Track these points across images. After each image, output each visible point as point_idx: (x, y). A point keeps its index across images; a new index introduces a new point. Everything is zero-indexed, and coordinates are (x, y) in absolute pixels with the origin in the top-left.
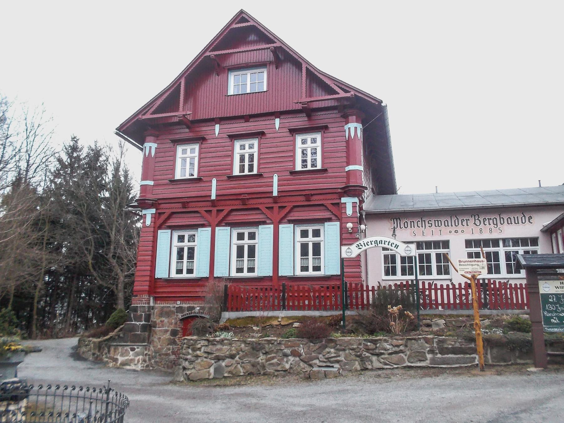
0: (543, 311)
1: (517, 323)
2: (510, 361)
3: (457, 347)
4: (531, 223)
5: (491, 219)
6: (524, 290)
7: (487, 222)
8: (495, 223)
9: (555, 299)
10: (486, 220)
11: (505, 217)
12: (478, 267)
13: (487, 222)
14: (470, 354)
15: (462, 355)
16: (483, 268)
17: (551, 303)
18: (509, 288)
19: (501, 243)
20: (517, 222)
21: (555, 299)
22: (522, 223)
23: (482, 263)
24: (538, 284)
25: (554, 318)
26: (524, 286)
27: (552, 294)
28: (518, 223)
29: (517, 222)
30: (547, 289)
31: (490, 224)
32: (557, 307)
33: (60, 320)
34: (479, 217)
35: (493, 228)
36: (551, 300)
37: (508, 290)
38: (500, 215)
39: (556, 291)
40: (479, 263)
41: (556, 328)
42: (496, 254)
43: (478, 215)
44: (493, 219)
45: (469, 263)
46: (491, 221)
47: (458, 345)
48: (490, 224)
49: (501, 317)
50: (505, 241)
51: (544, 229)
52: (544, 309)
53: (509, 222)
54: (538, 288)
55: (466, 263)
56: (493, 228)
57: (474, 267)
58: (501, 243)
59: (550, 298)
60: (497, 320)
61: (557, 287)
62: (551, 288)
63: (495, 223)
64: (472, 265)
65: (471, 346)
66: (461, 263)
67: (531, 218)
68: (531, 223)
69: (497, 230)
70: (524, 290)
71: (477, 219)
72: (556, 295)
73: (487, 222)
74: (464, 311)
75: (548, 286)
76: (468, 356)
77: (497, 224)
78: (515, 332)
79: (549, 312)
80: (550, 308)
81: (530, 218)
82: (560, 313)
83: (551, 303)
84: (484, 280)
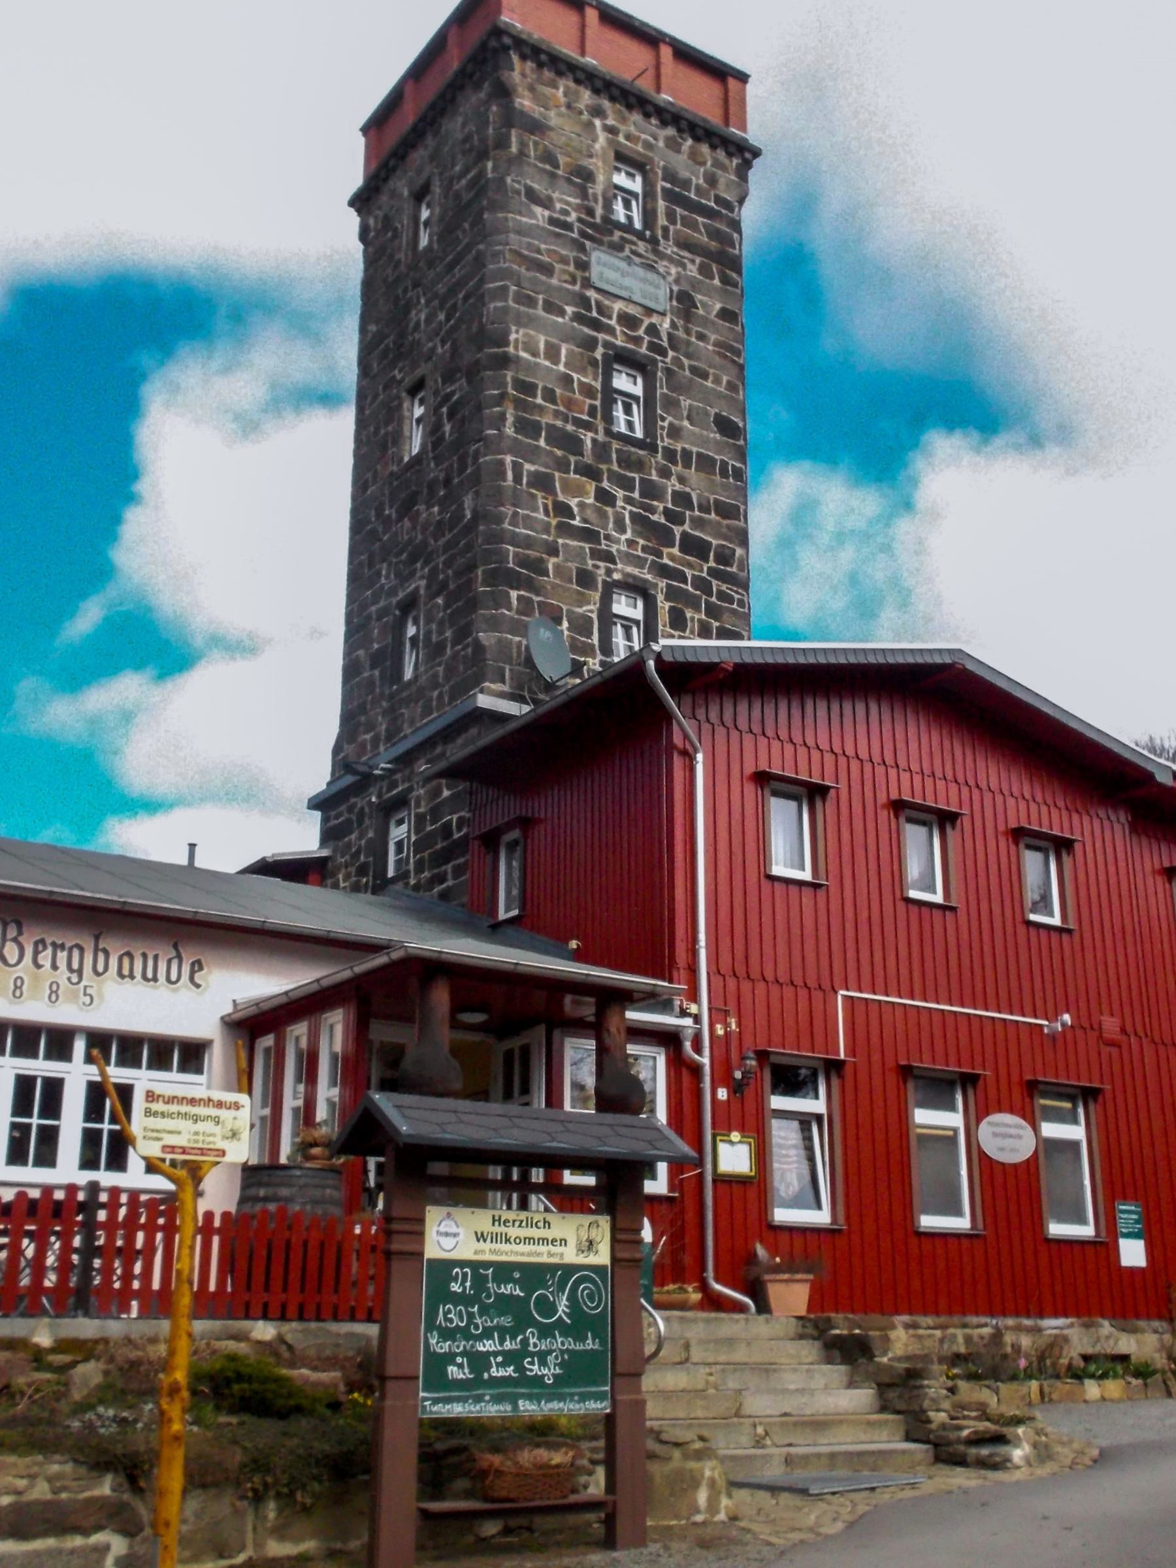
0: (427, 1330)
1: (240, 1377)
2: (242, 1548)
3: (37, 1502)
4: (198, 986)
5: (62, 947)
6: (216, 1240)
7: (45, 958)
8: (75, 966)
9: (468, 1284)
10: (45, 948)
11: (115, 946)
12: (217, 1130)
13: (45, 958)
14: (86, 1532)
15: (51, 1542)
16: (234, 1135)
17: (457, 1299)
18: (143, 1227)
19: (79, 1046)
20: (150, 975)
21: (468, 1284)
22: (168, 980)
23: (232, 1113)
24: (421, 1221)
25: (459, 1360)
26: (217, 1223)
27: (462, 1264)
28: (155, 979)
29: (150, 975)
30: (448, 1243)
31: (55, 967)
32: (471, 1316)
33: (106, 1409)
34: (20, 933)
35: (63, 982)
36: (455, 1287)
37: (159, 1236)
38: (97, 938)
39: (476, 1253)
40: (224, 1114)
41: (458, 1400)
42: (54, 1088)
43: (19, 926)
44: (71, 950)
45: (184, 1108)
46: (62, 956)
47: (41, 1491)
48: (55, 967)
49: (143, 1349)
50: (99, 1042)
51: (234, 1017)
52: (431, 1326)
53: (126, 972)
54: (420, 1235)
55: (174, 1108)
56: (63, 982)
57: (201, 1126)
58: (79, 1046)
59: (455, 1279)
60: (134, 1364)
61: (480, 1237)
62: (461, 1237)
63: (75, 966)
64: (196, 1119)
65: (96, 1492)
66: (155, 1107)
67: (201, 968)
68: (198, 986)
69: (78, 990)
70: (216, 1240)
71: (15, 940)
72: (475, 1265)
73: (45, 958)
74: (342, 1324)
75: (454, 1230)
76: (78, 1541)
77: (80, 972)
78: (246, 1418)
79: (447, 1334)
80: (451, 1321)
81: (197, 966)
82: (479, 1338)
83: (457, 1299)
84: (72, 1189)
